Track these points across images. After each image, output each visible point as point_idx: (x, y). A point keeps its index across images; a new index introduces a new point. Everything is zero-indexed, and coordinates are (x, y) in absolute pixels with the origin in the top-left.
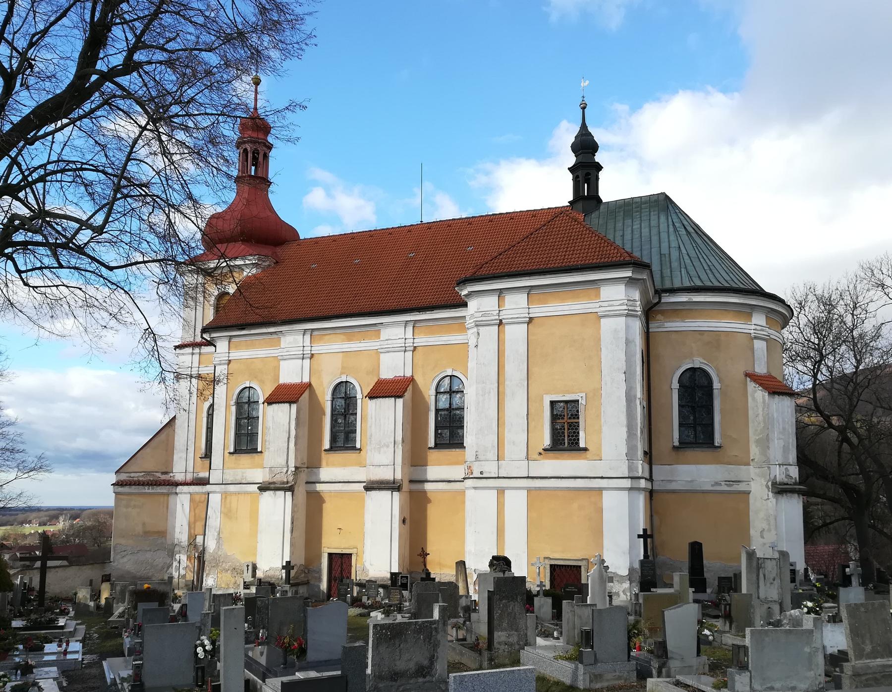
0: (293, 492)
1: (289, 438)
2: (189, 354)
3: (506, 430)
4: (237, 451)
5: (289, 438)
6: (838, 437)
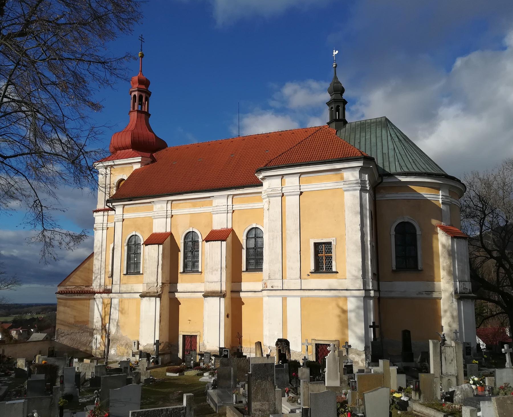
1: (158, 265)
2: (101, 215)
5: (158, 265)
6: (497, 263)
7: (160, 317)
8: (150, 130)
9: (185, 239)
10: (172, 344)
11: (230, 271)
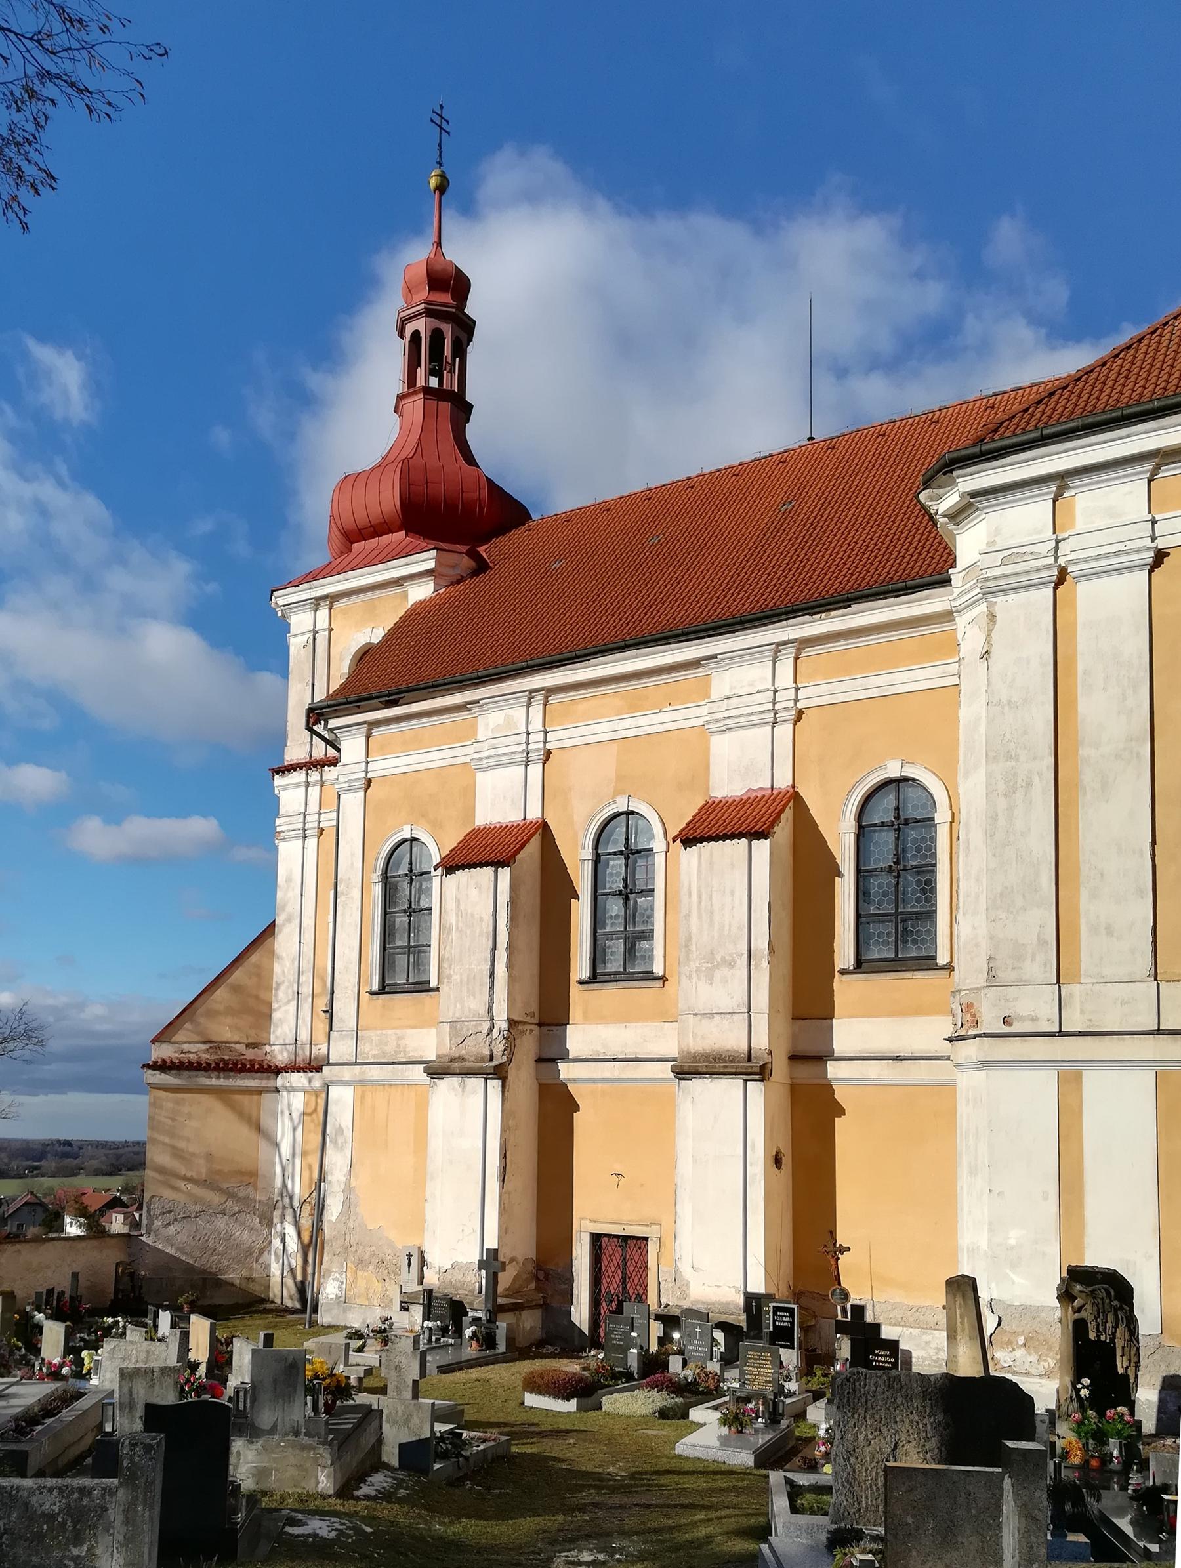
0: (504, 1079)
2: (297, 785)
3: (1084, 894)
4: (383, 990)
5: (494, 948)
7: (504, 1156)
8: (470, 459)
9: (596, 846)
10: (548, 1274)
11: (786, 968)
